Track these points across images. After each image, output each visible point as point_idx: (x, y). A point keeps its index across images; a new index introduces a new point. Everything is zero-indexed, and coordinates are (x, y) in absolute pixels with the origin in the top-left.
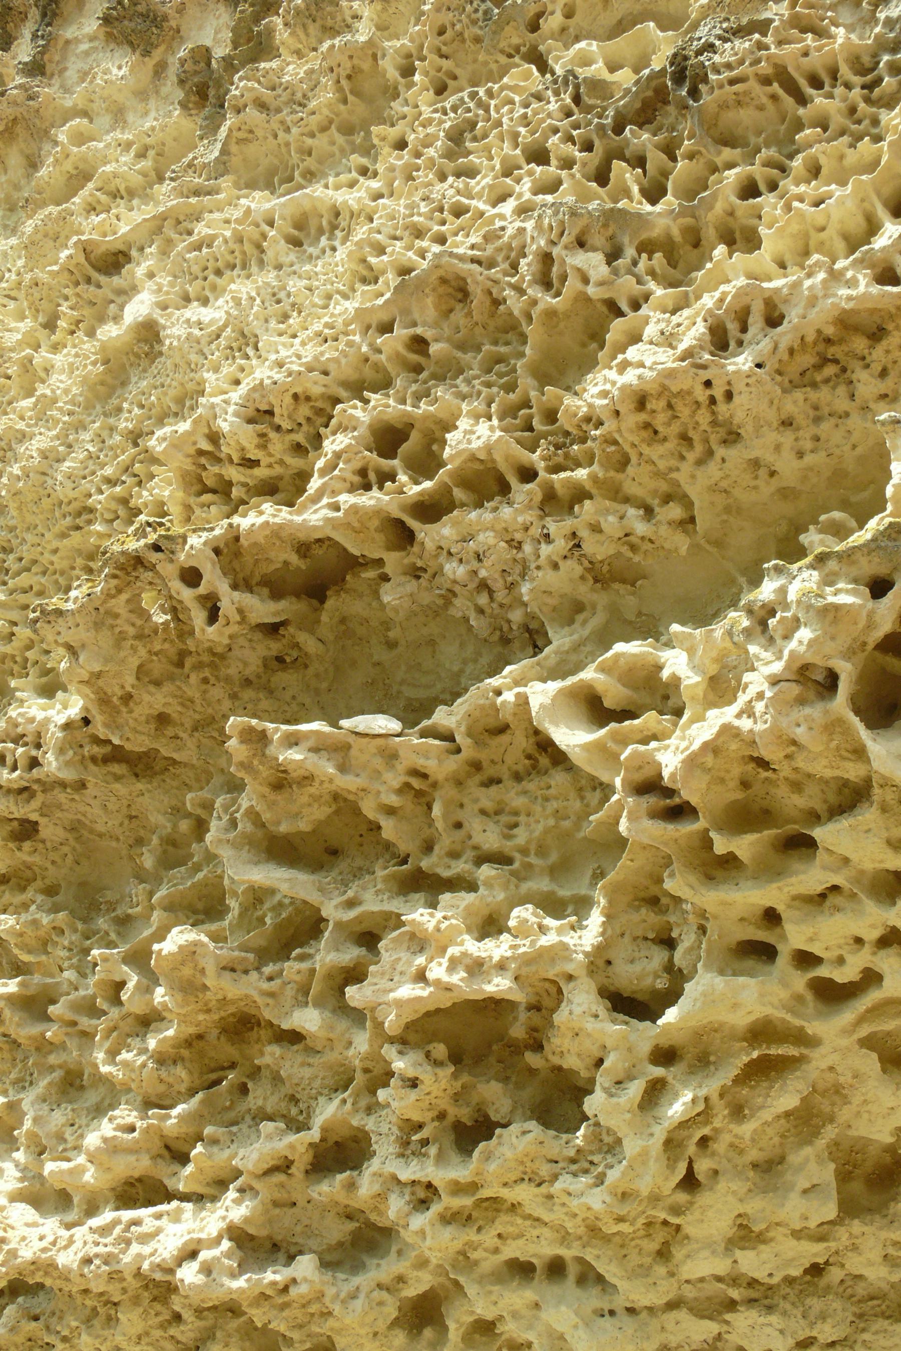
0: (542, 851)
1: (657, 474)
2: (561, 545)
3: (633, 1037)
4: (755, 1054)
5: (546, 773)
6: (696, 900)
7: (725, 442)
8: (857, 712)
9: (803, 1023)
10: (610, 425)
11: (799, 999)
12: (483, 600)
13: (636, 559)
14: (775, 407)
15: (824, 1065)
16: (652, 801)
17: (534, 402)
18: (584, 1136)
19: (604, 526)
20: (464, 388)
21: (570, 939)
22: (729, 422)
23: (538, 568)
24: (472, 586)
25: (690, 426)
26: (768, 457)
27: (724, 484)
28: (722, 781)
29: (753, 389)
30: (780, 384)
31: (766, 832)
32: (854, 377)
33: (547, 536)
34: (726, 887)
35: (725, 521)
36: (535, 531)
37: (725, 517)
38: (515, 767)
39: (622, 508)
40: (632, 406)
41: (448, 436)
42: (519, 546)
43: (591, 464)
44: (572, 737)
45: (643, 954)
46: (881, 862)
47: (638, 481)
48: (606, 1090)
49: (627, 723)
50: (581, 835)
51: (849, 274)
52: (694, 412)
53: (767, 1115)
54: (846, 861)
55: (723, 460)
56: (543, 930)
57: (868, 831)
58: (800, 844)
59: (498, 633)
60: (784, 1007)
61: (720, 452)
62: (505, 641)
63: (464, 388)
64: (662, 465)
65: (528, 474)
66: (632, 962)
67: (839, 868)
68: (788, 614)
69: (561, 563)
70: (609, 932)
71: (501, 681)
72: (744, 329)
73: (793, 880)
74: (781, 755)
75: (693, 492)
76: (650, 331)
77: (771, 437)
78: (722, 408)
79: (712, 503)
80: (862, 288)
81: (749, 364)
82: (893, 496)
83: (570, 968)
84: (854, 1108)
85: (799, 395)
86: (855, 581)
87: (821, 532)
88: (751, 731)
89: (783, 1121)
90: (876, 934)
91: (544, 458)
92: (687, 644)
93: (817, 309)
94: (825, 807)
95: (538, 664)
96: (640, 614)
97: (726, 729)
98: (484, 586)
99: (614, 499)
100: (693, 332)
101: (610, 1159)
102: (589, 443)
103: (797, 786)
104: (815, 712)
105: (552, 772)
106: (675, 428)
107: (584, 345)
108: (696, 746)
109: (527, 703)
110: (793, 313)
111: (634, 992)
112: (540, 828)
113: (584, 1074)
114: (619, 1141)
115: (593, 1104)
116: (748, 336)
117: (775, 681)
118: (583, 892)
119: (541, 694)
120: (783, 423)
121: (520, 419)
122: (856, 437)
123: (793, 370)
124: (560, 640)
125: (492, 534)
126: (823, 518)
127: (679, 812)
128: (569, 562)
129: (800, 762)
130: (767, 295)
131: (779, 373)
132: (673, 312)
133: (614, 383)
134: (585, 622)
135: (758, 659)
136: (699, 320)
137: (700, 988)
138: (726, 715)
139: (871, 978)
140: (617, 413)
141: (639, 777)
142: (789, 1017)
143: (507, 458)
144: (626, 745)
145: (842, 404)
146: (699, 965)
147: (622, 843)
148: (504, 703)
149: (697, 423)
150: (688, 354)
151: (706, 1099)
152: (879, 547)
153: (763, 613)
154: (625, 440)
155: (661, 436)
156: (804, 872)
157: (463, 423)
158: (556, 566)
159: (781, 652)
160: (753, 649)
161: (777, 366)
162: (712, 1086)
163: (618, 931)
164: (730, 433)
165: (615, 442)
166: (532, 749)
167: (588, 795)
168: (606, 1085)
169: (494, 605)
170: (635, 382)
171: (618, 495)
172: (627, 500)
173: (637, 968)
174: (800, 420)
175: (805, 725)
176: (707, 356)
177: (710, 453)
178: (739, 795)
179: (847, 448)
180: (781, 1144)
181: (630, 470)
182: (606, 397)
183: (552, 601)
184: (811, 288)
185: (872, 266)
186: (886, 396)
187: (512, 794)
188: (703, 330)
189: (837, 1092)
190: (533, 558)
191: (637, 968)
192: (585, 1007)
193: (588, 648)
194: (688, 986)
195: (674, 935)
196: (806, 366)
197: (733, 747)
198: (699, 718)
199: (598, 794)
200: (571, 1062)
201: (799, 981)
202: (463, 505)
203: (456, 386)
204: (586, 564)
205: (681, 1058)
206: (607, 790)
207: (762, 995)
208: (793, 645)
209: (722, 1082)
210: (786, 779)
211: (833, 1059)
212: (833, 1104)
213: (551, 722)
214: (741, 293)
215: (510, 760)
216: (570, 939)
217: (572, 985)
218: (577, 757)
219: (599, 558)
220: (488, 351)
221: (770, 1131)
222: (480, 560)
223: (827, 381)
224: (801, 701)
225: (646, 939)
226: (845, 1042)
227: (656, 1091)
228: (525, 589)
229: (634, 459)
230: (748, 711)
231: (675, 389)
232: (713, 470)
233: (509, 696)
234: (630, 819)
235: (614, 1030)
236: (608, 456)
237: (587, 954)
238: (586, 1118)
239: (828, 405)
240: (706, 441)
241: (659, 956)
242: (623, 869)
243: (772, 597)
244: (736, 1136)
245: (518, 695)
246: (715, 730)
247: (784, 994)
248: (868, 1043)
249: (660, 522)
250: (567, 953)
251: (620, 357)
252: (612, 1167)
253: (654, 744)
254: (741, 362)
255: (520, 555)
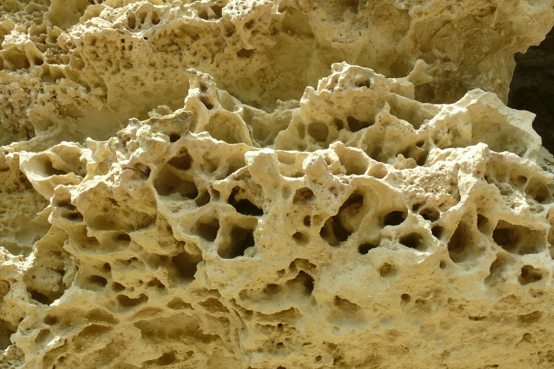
0: (14, 225)
1: (95, 74)
2: (47, 95)
3: (38, 310)
4: (90, 324)
5: (22, 192)
6: (76, 255)
7: (126, 67)
8: (156, 187)
9: (113, 314)
10: (79, 48)
11: (113, 303)
12: (8, 112)
13: (79, 108)
14: (148, 57)
15: (118, 332)
16: (64, 210)
17: (48, 31)
18: (8, 351)
19: (68, 91)
20: (18, 18)
21: (18, 264)
22: (128, 59)
23: (36, 103)
24: (5, 104)
25: (112, 57)
26: (142, 77)
27: (122, 84)
28: (96, 206)
29: (141, 47)
30: (153, 48)
31: (110, 231)
32: (183, 52)
33: (42, 90)
34: (90, 251)
35: (120, 100)
36: (38, 87)
37: (120, 98)
38: (9, 187)
39: (78, 85)
40: (89, 43)
41: (6, 36)
42: (29, 92)
43: (67, 63)
44: (35, 177)
45: (50, 275)
46: (155, 250)
47: (86, 75)
48: (21, 332)
49: (61, 175)
50: (33, 221)
51: (189, 10)
52: (115, 51)
53: (91, 350)
54: (141, 248)
55: (123, 74)
56: (6, 258)
57: (152, 236)
58: (124, 239)
59: (13, 128)
60: (105, 306)
61: (123, 70)
62: (15, 132)
63: (18, 18)
64: (98, 70)
65: (39, 62)
66: (44, 278)
67: (138, 251)
68: (135, 141)
69: (46, 103)
70: (36, 264)
71: (9, 148)
72: (143, 22)
73: (118, 253)
74: (122, 199)
75: (108, 85)
76: (103, 13)
77: (145, 69)
78: (127, 52)
79: (116, 92)
80: (193, 17)
81: (141, 37)
82: (187, 102)
83: (15, 277)
84: (127, 351)
85: (159, 54)
86: (165, 133)
87: (157, 112)
88: (111, 187)
89: (97, 354)
90: (148, 280)
91: (47, 56)
92: (93, 147)
93: (173, 21)
94: (137, 224)
95: (28, 144)
96: (77, 132)
97: (101, 185)
98: (10, 106)
99: (75, 81)
100: (121, 18)
101: (18, 362)
102: (68, 54)
103: (126, 214)
104: (139, 183)
105: (25, 192)
106: (105, 57)
107: (75, 13)
108: (87, 189)
109: (19, 159)
110: (164, 20)
111: (43, 291)
112: (15, 215)
113: (14, 324)
114: (23, 355)
115: (14, 338)
116: (143, 25)
117: (124, 168)
118: (29, 246)
119: (25, 156)
120: (151, 64)
121: (39, 36)
122: (179, 77)
123: (160, 43)
124: (39, 136)
125: (18, 84)
126: (159, 107)
127: (76, 217)
128: (50, 103)
129: (129, 204)
130: (155, 10)
131: (153, 43)
132: (115, 8)
133: (83, 31)
134: (52, 131)
135: (119, 157)
136: (125, 13)
137: (71, 293)
138: (103, 178)
139: (143, 298)
140: (83, 44)
141: (61, 199)
142: (107, 310)
143: (31, 52)
144: (58, 184)
145: (176, 62)
146: (73, 283)
147: (49, 226)
148: (9, 157)
149: (116, 56)
150: (117, 26)
151: (66, 341)
152: (177, 121)
153: (125, 139)
154: (84, 57)
155: (99, 58)
156: (123, 250)
157: (14, 33)
158: (43, 104)
159: (129, 156)
160: (118, 153)
161: (153, 40)
162: (69, 335)
163: (41, 264)
164: (128, 64)
165: (80, 57)
166: (18, 180)
167: (39, 204)
168: (22, 330)
169: (13, 115)
170: (93, 32)
171: (76, 79)
172: (80, 82)
173: (46, 281)
174: (158, 65)
175: (134, 187)
176: (125, 29)
177: (119, 70)
178: (102, 214)
179: (175, 81)
180: (95, 363)
181: (84, 70)
182: (79, 36)
183: (40, 119)
184: (173, 12)
185: (198, 9)
186: (194, 63)
187: (5, 198)
188: (125, 18)
189: (122, 344)
190: (34, 98)
191: (46, 281)
192: (18, 295)
193: (51, 142)
194: (66, 292)
195: (65, 269)
196: (165, 43)
197: (103, 192)
198: (92, 178)
199: (43, 204)
200: (8, 318)
201: (114, 296)
202: (7, 68)
203: (14, 16)
204: (57, 106)
205: (58, 322)
206: (47, 202)
207: (97, 299)
208: (135, 154)
209: (74, 334)
210: (123, 210)
211: (122, 330)
212: (120, 349)
213: (28, 169)
214: (144, 6)
215: (7, 183)
216: (18, 264)
217: (15, 284)
218: (36, 186)
219: (63, 104)
220: (32, 5)
221: (91, 358)
222: (10, 94)
223: (172, 51)
224: (134, 178)
225: (52, 269)
226: (128, 323)
227: (44, 335)
228: (28, 111)
229: (86, 65)
230: (111, 179)
231: (109, 40)
232: (118, 77)
233: (11, 155)
234: (54, 216)
235: (30, 306)
236: (75, 62)
237: (24, 272)
238: (11, 344)
239: (171, 61)
240: (118, 65)
241: (56, 277)
242: (48, 237)
243: (130, 133)
244: (76, 358)
245: (15, 155)
246: (96, 184)
247: (106, 300)
248: (138, 325)
249: (92, 94)
250: (15, 270)
251: (89, 21)
252: (18, 366)
253: (70, 186)
254: (139, 35)
255: (29, 96)
